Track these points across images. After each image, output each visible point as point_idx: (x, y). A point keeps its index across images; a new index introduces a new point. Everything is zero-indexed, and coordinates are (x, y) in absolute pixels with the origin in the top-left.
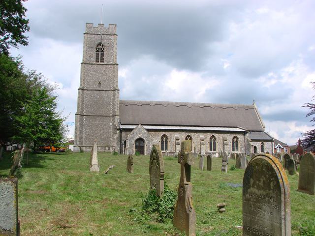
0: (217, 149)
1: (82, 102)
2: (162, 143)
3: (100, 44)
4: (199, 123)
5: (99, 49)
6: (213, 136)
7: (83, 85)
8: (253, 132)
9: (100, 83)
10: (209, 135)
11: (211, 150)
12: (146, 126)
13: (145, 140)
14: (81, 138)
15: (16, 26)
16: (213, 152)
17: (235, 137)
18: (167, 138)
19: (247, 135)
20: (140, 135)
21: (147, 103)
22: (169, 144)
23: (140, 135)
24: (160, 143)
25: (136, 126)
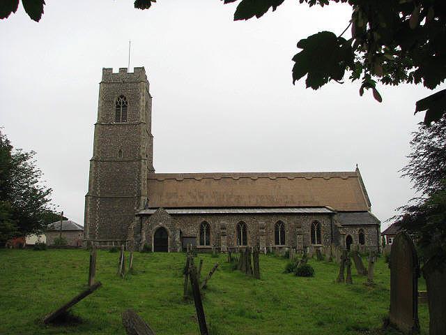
0: (286, 241)
1: (96, 178)
2: (201, 234)
3: (122, 97)
4: (214, 203)
5: (120, 103)
6: (280, 222)
7: (96, 155)
8: (351, 214)
9: (120, 151)
10: (274, 221)
11: (277, 243)
12: (289, 209)
13: (169, 230)
14: (92, 229)
15: (383, 47)
16: (280, 246)
17: (242, 223)
18: (283, 226)
19: (335, 217)
20: (161, 224)
21: (173, 177)
22: (249, 236)
23: (161, 224)
24: (198, 234)
25: (155, 210)
